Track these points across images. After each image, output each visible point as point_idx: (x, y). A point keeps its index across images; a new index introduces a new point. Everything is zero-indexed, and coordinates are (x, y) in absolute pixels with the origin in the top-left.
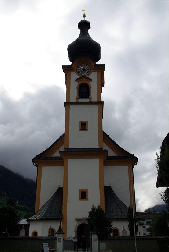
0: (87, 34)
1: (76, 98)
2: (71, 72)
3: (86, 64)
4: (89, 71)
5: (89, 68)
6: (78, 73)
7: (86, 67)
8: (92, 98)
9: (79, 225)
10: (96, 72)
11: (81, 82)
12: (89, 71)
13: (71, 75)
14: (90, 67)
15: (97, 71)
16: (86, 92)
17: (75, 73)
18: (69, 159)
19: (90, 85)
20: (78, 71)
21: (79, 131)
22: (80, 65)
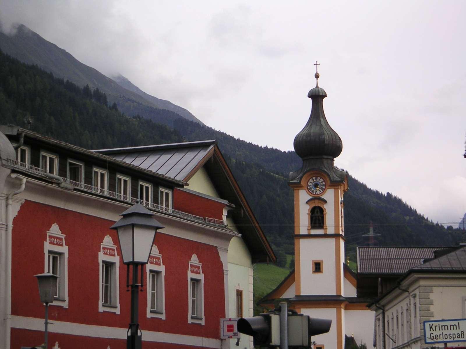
0: (321, 116)
1: (308, 229)
2: (299, 239)
3: (319, 177)
4: (324, 187)
5: (324, 183)
6: (309, 190)
7: (320, 180)
8: (327, 229)
9: (311, 208)
10: (333, 189)
11: (313, 206)
12: (324, 187)
13: (300, 243)
14: (324, 181)
15: (334, 188)
16: (320, 218)
17: (304, 190)
18: (301, 309)
19: (325, 209)
20: (309, 187)
21: (313, 273)
22: (312, 178)
